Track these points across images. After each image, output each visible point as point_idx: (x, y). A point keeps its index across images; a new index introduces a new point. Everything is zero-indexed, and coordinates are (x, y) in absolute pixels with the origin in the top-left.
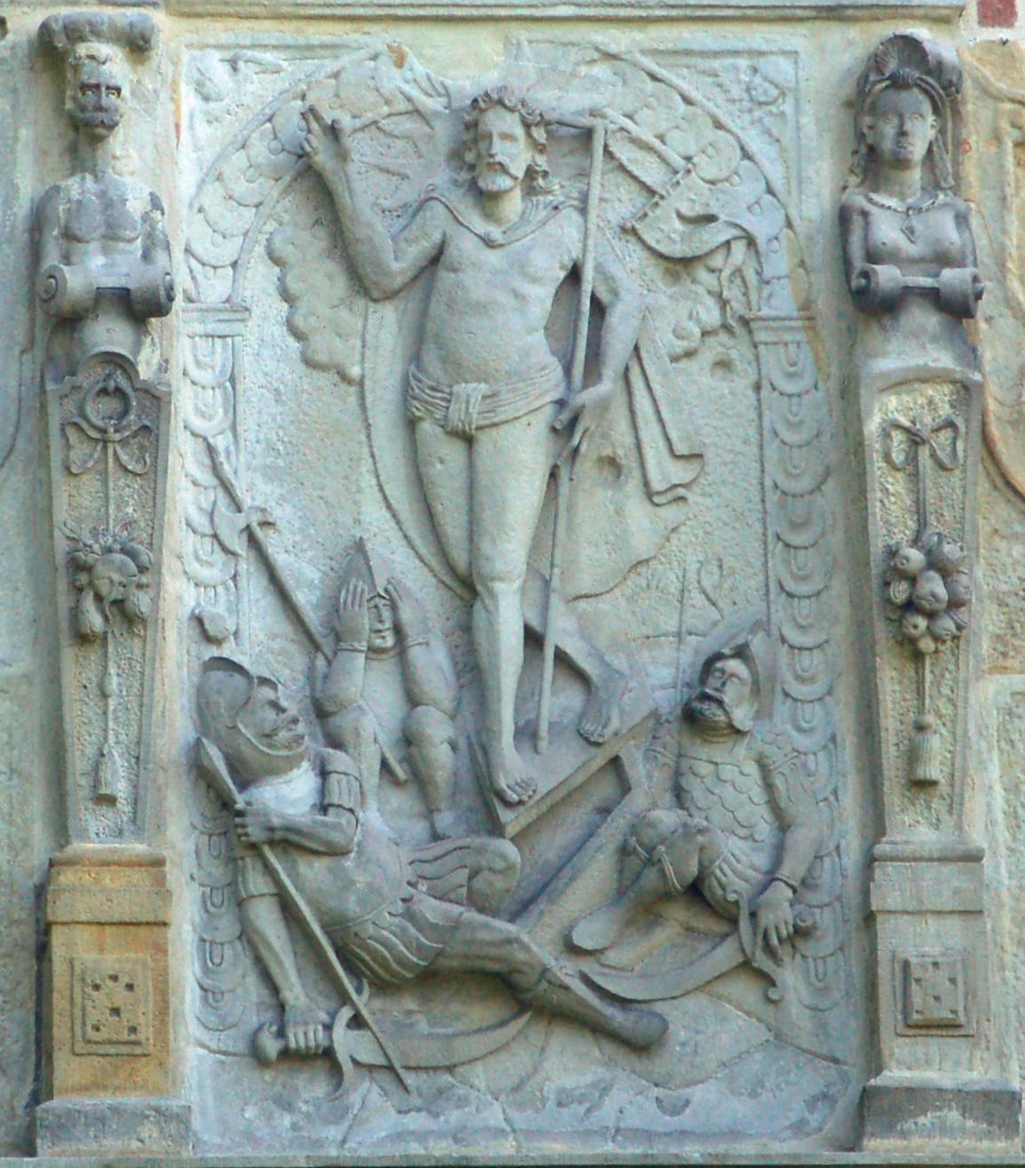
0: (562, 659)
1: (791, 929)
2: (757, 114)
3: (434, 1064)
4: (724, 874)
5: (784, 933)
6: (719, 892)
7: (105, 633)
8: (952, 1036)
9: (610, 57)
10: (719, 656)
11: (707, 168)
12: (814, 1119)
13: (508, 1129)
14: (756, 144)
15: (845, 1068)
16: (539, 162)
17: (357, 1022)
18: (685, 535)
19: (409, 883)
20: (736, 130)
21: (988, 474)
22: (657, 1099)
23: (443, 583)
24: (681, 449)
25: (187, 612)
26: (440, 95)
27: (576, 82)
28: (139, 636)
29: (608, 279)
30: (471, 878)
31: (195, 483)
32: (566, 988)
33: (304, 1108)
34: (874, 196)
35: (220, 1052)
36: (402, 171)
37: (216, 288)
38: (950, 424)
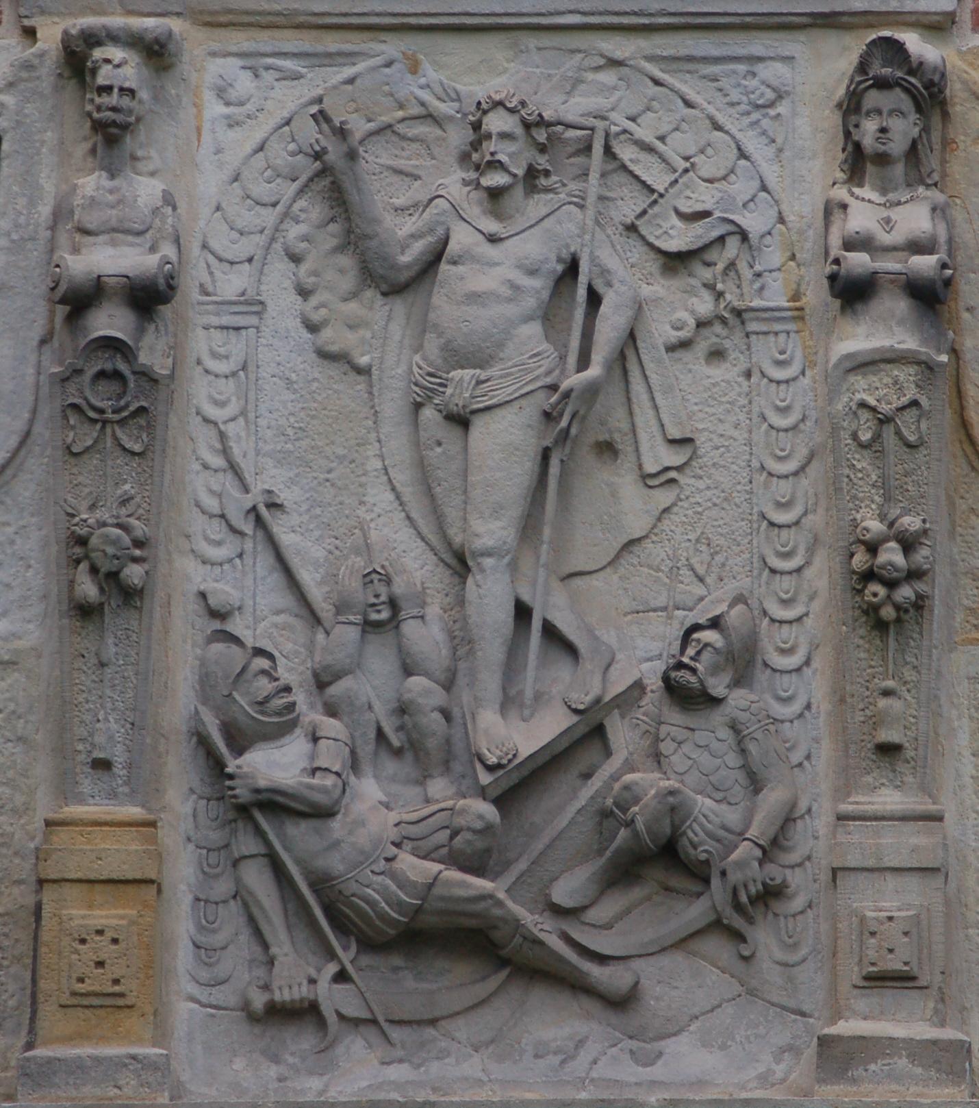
0: (551, 633)
1: (760, 887)
2: (755, 116)
3: (418, 1017)
4: (696, 835)
5: (753, 890)
6: (691, 851)
7: (102, 604)
8: (907, 988)
9: (614, 63)
10: (696, 628)
11: (707, 167)
12: (780, 1070)
13: (485, 1079)
14: (752, 144)
15: (811, 1020)
16: (540, 161)
17: (342, 977)
18: (676, 517)
19: (393, 843)
20: (734, 131)
21: (966, 456)
22: (631, 1051)
23: (442, 560)
24: (675, 433)
25: (195, 589)
26: (453, 100)
27: (583, 87)
28: (136, 607)
29: (604, 272)
30: (452, 838)
31: (206, 467)
32: (541, 943)
33: (291, 1060)
34: (856, 190)
35: (211, 1006)
36: (416, 172)
37: (232, 284)
38: (915, 403)
